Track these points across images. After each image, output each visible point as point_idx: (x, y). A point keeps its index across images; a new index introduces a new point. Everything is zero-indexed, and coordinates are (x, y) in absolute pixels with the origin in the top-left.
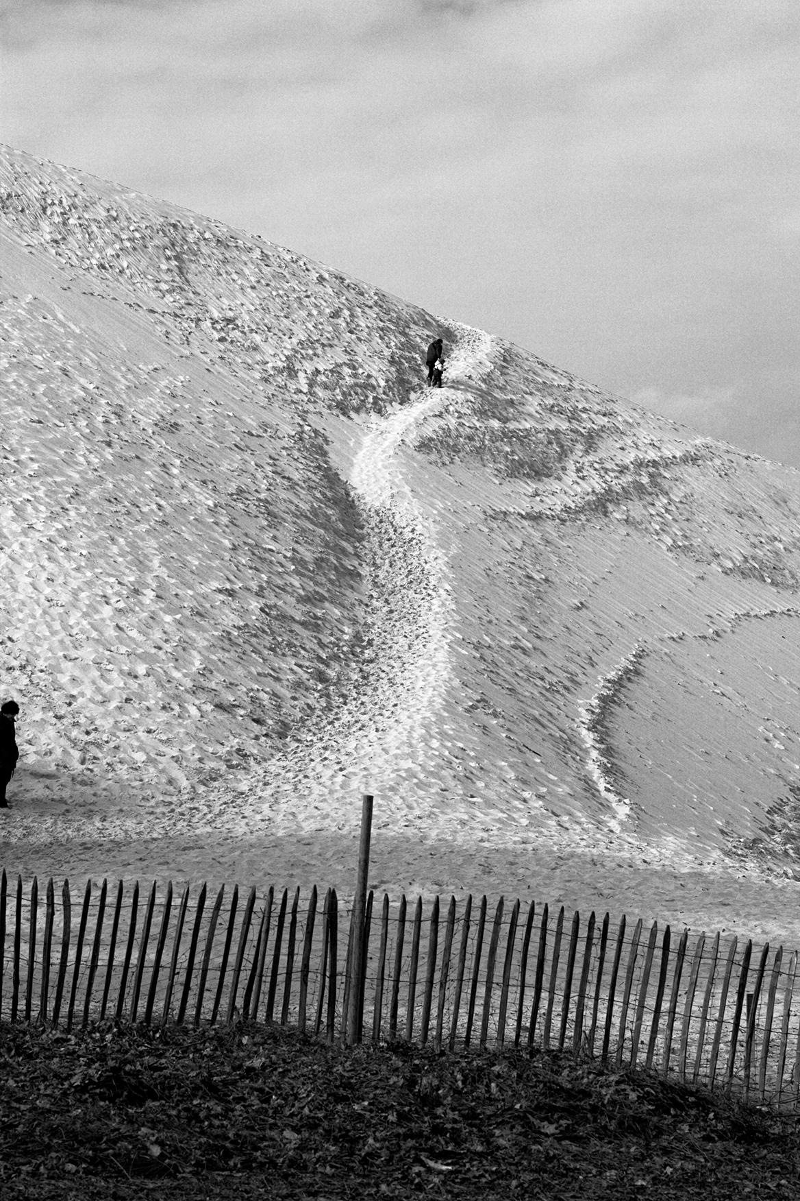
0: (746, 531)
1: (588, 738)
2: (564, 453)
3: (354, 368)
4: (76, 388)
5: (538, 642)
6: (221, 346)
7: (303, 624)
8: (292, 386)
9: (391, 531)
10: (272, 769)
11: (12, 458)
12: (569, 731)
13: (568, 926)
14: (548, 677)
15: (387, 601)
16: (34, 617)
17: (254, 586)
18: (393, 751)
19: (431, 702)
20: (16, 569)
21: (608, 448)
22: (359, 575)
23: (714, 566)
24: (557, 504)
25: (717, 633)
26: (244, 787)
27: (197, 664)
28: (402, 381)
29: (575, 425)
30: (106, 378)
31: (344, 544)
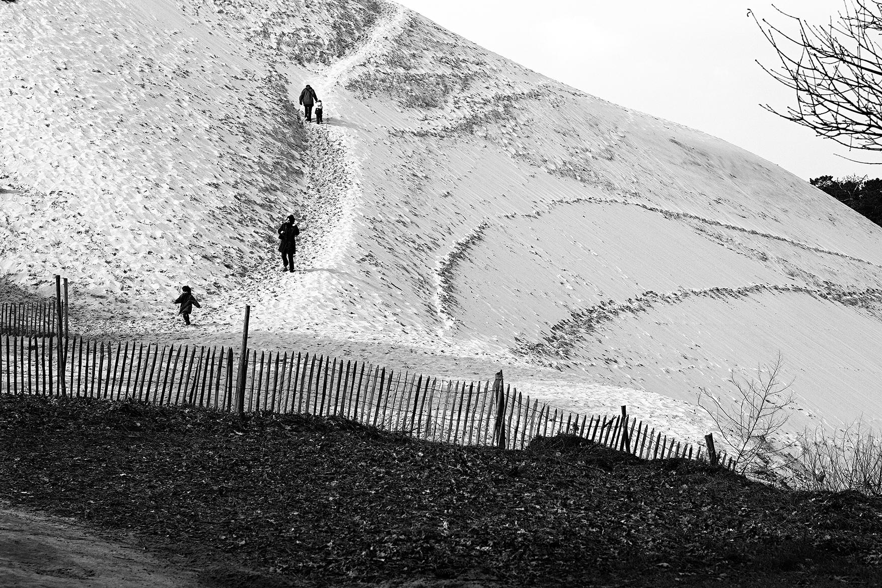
0: (567, 145)
1: (438, 280)
2: (446, 91)
3: (308, 32)
4: (123, 47)
5: (415, 219)
6: (220, 16)
7: (261, 206)
8: (266, 43)
9: (325, 144)
10: (235, 295)
11: (81, 96)
12: (425, 276)
13: (338, 367)
14: (418, 241)
15: (318, 191)
16: (94, 201)
17: (232, 181)
18: (308, 286)
19: (336, 257)
20: (83, 170)
21: (477, 88)
22: (302, 173)
23: (543, 169)
24: (439, 125)
25: (538, 213)
26: (216, 305)
27: (193, 230)
28: (340, 41)
29: (456, 71)
30: (142, 39)
31: (294, 152)
